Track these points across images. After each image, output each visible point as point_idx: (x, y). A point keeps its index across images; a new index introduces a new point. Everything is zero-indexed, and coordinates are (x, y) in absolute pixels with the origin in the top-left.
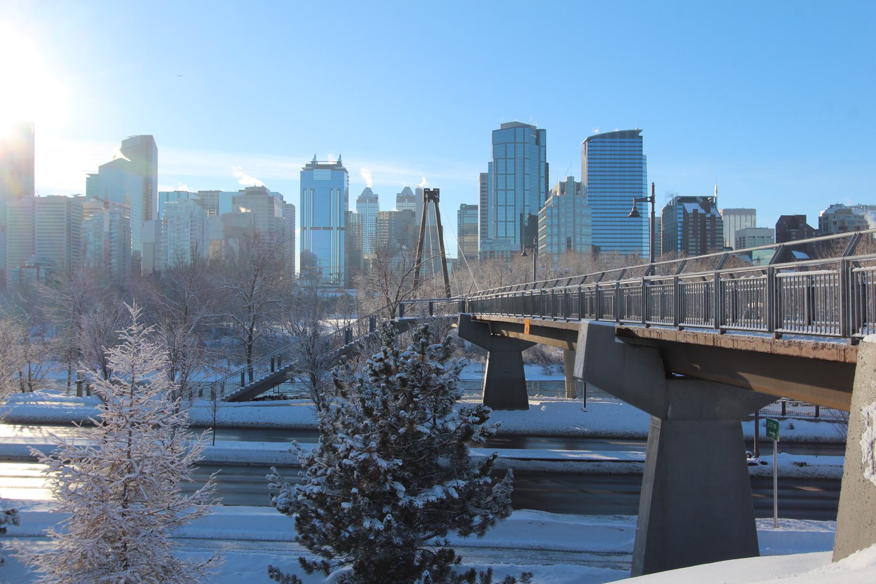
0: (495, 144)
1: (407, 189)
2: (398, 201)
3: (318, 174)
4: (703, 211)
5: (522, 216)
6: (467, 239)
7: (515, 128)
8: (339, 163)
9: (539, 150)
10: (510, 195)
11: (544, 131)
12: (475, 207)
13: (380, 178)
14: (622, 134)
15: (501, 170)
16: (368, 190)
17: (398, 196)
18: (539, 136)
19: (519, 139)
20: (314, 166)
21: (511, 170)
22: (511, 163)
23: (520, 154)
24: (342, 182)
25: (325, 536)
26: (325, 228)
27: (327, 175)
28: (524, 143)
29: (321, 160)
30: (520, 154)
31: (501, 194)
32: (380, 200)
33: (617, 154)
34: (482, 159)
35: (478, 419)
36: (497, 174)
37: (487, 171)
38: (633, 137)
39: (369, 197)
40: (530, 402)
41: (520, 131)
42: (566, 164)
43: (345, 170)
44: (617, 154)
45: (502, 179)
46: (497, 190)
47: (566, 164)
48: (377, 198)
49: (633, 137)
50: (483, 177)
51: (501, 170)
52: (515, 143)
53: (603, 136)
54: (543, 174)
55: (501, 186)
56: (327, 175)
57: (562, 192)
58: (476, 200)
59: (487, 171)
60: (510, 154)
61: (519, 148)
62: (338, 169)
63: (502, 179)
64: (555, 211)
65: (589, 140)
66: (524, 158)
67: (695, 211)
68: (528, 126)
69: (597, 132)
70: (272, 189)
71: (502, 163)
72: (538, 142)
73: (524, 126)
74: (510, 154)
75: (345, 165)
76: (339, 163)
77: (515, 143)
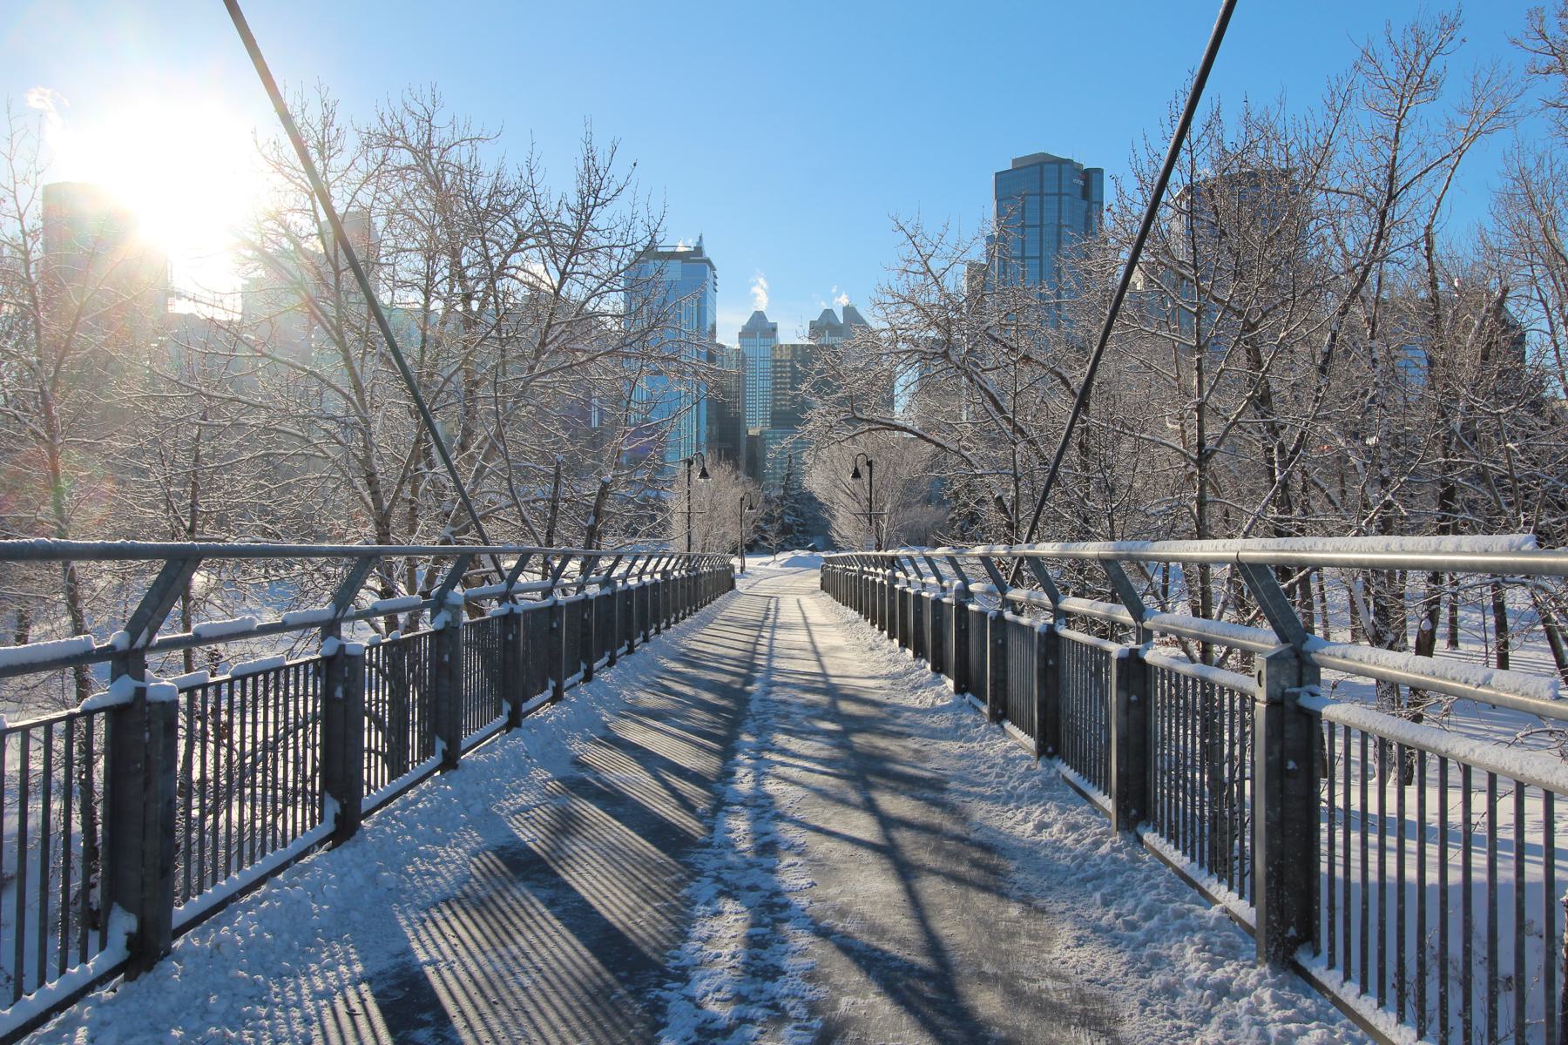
1: (828, 313)
7: (1041, 164)
8: (698, 250)
9: (1089, 209)
11: (1100, 171)
16: (759, 316)
19: (1051, 187)
24: (702, 283)
25: (1254, 326)
27: (674, 270)
28: (1060, 194)
34: (966, 225)
35: (1011, 755)
40: (1323, 676)
43: (708, 261)
48: (774, 330)
52: (1041, 194)
66: (1060, 226)
68: (1069, 162)
71: (1014, 236)
72: (1086, 193)
75: (708, 253)
76: (698, 250)
77: (1041, 194)
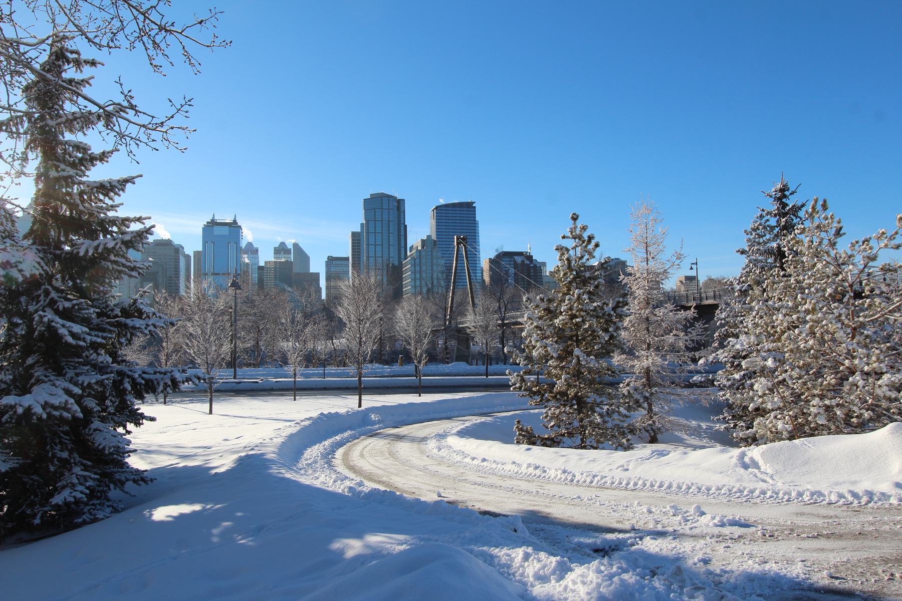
0: (366, 209)
1: (283, 244)
2: (275, 253)
3: (217, 230)
4: (528, 262)
5: (388, 265)
6: (332, 284)
8: (235, 221)
10: (379, 248)
12: (347, 259)
13: (264, 235)
14: (461, 205)
15: (372, 230)
17: (275, 249)
18: (400, 203)
19: (385, 206)
20: (213, 224)
21: (379, 230)
22: (379, 224)
23: (385, 217)
26: (223, 274)
27: (225, 231)
29: (219, 218)
30: (385, 217)
31: (372, 248)
32: (259, 253)
33: (458, 220)
34: (356, 221)
36: (368, 233)
37: (201, 249)
38: (469, 207)
39: (252, 250)
41: (385, 200)
42: (420, 229)
43: (240, 227)
44: (458, 220)
45: (372, 237)
46: (368, 245)
47: (420, 229)
49: (469, 207)
50: (355, 236)
51: (372, 230)
53: (447, 206)
54: (403, 233)
55: (372, 241)
56: (225, 231)
57: (423, 247)
58: (347, 252)
59: (201, 249)
60: (378, 217)
61: (385, 212)
62: (234, 226)
63: (372, 237)
64: (417, 261)
65: (436, 208)
67: (523, 261)
69: (442, 202)
70: (176, 242)
71: (372, 223)
73: (389, 196)
74: (378, 217)
